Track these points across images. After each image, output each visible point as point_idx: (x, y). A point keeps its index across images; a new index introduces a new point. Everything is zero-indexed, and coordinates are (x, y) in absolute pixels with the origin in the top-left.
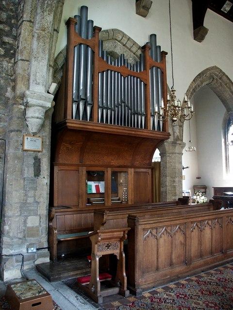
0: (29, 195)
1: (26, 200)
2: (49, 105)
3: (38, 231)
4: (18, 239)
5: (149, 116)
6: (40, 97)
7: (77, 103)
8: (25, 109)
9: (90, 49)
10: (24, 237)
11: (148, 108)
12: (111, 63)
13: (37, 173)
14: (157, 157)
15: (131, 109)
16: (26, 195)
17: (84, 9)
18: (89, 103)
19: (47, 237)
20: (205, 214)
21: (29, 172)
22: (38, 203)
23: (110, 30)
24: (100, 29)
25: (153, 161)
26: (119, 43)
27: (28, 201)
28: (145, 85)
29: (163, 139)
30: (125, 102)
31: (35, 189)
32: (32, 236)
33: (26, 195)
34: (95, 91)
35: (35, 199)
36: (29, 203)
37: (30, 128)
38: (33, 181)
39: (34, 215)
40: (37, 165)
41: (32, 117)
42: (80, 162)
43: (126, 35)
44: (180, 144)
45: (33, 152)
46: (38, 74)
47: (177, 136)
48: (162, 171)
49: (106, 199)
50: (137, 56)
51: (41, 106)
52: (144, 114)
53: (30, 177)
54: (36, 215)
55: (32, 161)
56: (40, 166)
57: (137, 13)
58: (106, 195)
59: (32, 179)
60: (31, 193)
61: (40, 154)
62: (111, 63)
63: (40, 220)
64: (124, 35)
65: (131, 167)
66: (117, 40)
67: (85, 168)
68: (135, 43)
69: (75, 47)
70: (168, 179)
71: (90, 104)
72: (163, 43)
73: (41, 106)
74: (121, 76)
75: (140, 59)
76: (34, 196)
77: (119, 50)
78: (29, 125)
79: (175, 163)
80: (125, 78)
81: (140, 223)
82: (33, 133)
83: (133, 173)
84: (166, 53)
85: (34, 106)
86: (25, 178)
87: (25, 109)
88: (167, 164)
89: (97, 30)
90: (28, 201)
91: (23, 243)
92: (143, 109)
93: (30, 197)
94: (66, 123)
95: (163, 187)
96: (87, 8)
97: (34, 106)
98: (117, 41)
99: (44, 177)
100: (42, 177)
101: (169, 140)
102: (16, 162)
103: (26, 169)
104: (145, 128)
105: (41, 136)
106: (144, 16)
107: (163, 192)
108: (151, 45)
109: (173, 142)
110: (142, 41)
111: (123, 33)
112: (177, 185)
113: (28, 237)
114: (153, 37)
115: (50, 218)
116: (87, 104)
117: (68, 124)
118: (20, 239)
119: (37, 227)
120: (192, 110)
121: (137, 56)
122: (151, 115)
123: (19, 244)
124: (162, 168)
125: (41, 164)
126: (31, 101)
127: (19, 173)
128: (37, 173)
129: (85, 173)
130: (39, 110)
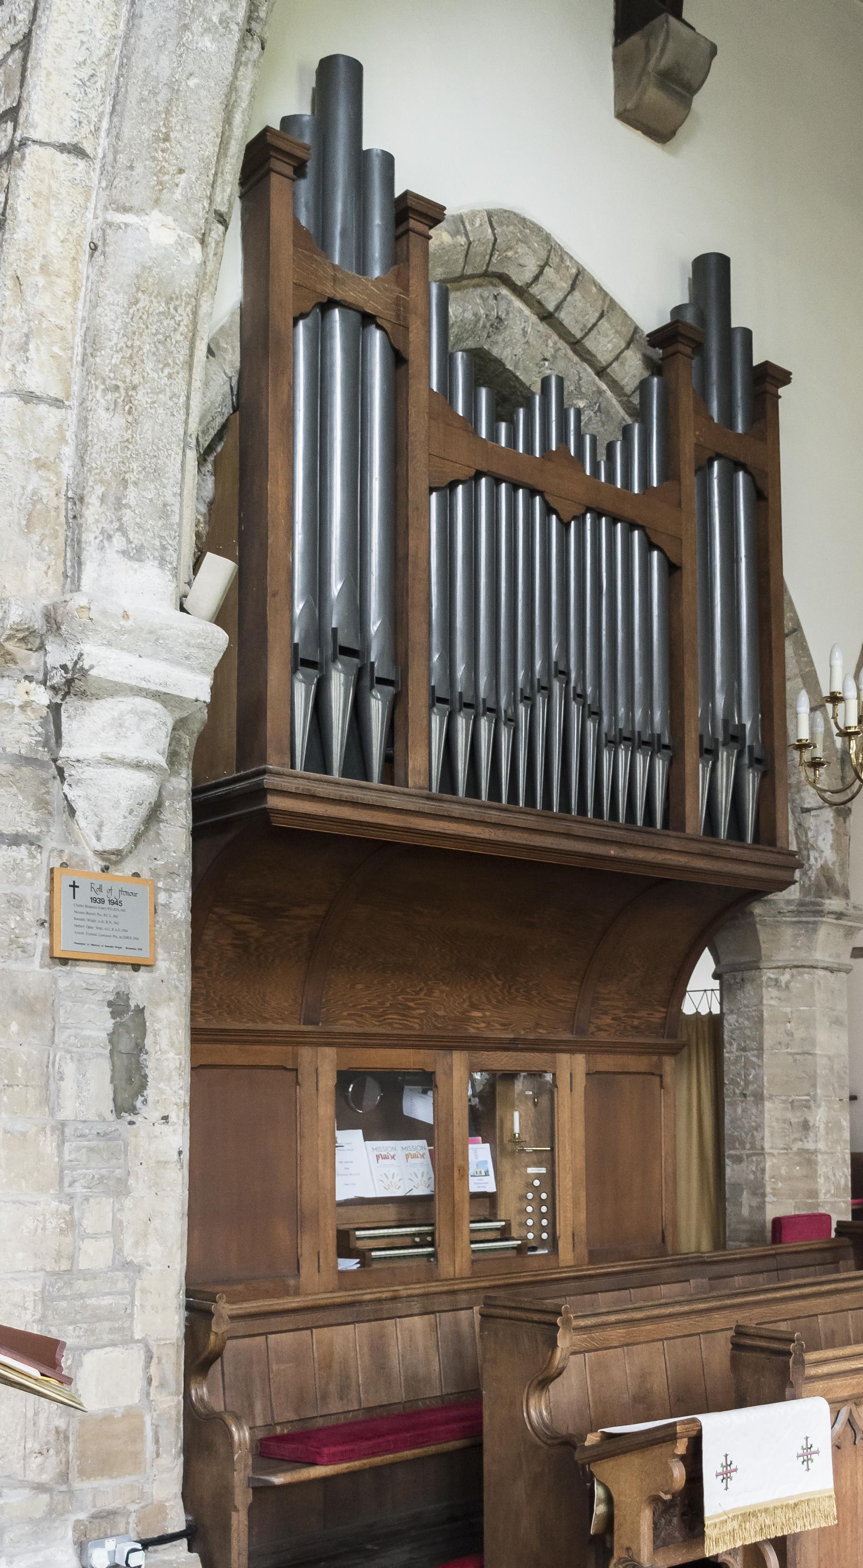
0: (89, 1223)
1: (72, 1258)
2: (198, 687)
3: (136, 1435)
4: (27, 1492)
5: (691, 753)
6: (153, 640)
7: (314, 673)
8: (55, 709)
9: (377, 338)
10: (64, 1477)
11: (688, 705)
12: (494, 434)
13: (130, 1087)
14: (701, 994)
15: (597, 714)
16: (71, 1225)
17: (339, 81)
18: (377, 674)
19: (182, 1459)
20: (520, 1277)
21: (87, 1088)
22: (132, 1269)
23: (474, 214)
24: (433, 214)
25: (688, 1009)
26: (518, 303)
27: (83, 1264)
28: (671, 569)
29: (751, 886)
30: (566, 673)
31: (120, 1188)
32: (105, 1465)
33: (71, 1225)
34: (692, 665)
35: (118, 1250)
36: (90, 1275)
37: (84, 822)
38: (111, 1145)
39: (115, 1345)
40: (125, 1044)
41: (110, 761)
42: (307, 1022)
43: (563, 255)
44: (840, 915)
45: (102, 971)
46: (132, 496)
47: (824, 869)
48: (730, 1070)
49: (443, 1235)
50: (614, 385)
51: (156, 696)
52: (666, 740)
53: (92, 1116)
54: (128, 1341)
55: (101, 1024)
56: (140, 1048)
57: (623, 115)
58: (439, 1207)
59: (102, 1128)
60: (97, 1214)
61: (142, 977)
62: (494, 434)
63: (147, 1365)
64: (552, 253)
65: (572, 1048)
66: (505, 280)
67: (330, 1053)
68: (609, 308)
69: (295, 324)
70: (772, 1111)
71: (381, 681)
72: (767, 316)
73: (156, 696)
74: (548, 510)
75: (641, 414)
76: (118, 1229)
77: (523, 346)
78: (80, 806)
79: (809, 1022)
80: (564, 526)
81: (811, 1371)
82: (101, 854)
83: (580, 1081)
84: (784, 377)
85: (115, 690)
86: (63, 1124)
87: (55, 709)
88: (767, 1027)
89: (413, 215)
90: (83, 1264)
91: (54, 1513)
92: (658, 715)
93: (95, 1236)
94: (261, 793)
95: (738, 1159)
96: (356, 69)
97: (115, 690)
98: (505, 291)
99: (165, 1118)
100: (158, 1115)
101: (40, 772)
102: (14, 1027)
103: (70, 1069)
104: (666, 824)
105: (145, 874)
106: (661, 132)
107: (738, 1188)
108: (702, 318)
109: (802, 904)
110: (651, 296)
111: (547, 238)
112: (821, 1146)
113: (83, 1473)
114: (712, 275)
115: (199, 1359)
116: (366, 682)
117: (274, 802)
118: (40, 1488)
119: (130, 1413)
120: (851, 718)
121: (614, 385)
122: (300, 662)
123: (31, 1520)
124: (730, 1052)
125: (148, 1042)
126: (104, 661)
127: (32, 1095)
128: (130, 1087)
129: (328, 1081)
130: (142, 716)
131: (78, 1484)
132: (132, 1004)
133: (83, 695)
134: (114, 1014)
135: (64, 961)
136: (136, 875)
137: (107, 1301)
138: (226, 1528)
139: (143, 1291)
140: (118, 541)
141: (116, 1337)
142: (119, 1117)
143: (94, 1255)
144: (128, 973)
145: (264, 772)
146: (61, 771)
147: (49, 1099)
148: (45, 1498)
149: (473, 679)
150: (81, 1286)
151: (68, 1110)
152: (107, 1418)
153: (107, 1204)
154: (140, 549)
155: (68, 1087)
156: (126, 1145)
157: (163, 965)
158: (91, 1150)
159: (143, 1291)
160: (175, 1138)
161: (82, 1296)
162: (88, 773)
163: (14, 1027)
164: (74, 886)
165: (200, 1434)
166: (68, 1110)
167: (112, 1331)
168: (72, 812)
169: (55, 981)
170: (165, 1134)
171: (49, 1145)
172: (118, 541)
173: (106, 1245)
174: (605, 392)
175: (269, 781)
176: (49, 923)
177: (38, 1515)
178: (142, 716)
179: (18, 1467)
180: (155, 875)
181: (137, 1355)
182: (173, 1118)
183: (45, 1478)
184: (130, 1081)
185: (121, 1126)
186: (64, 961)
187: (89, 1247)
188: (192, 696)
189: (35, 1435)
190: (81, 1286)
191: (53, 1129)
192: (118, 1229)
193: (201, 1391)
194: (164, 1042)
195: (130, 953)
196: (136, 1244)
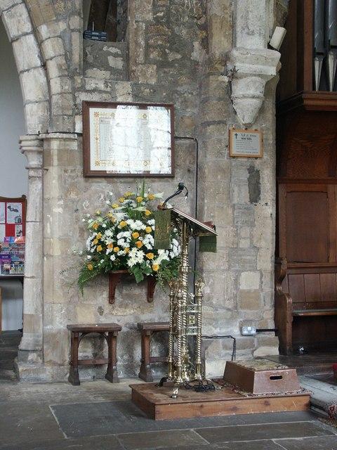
0: (243, 234)
2: (272, 71)
3: (258, 298)
10: (236, 307)
13: (255, 196)
21: (241, 195)
31: (252, 225)
32: (248, 306)
33: (237, 235)
35: (251, 243)
37: (239, 116)
39: (250, 271)
45: (246, 160)
51: (259, 75)
55: (245, 175)
60: (245, 232)
61: (258, 161)
63: (261, 278)
76: (251, 237)
78: (238, 111)
82: (245, 125)
85: (246, 75)
86: (234, 205)
93: (244, 238)
97: (246, 75)
99: (266, 204)
103: (236, 189)
105: (259, 129)
115: (279, 278)
117: (306, 102)
126: (242, 67)
127: (225, 197)
128: (255, 196)
130: (255, 82)
131: (240, 310)
132: (255, 169)
133: (237, 78)
134: (249, 173)
135: (234, 157)
136: (256, 130)
137: (248, 257)
138: (285, 330)
139: (260, 256)
140: (246, 30)
141: (251, 268)
142: (251, 203)
143: (244, 244)
144: (254, 160)
145: (302, 93)
146: (232, 101)
147: (230, 198)
148: (230, 313)
149: (131, 180)
150: (240, 252)
151: (235, 201)
152: (249, 292)
153: (248, 229)
154: (253, 32)
155: (236, 194)
156: (254, 211)
157: (266, 157)
158: (243, 213)
159: (260, 256)
160: (270, 210)
161: (241, 256)
162: (239, 101)
163: (219, 177)
164: (236, 135)
165: (279, 301)
166: (235, 201)
167: (250, 266)
168: (236, 113)
169: (231, 163)
170: (267, 209)
171: (230, 212)
172: (246, 30)
173: (248, 241)
174: (60, 239)
175: (303, 96)
176: (229, 146)
177: (228, 317)
178: (255, 82)
179: (222, 303)
180: (262, 129)
181: (257, 275)
182: (269, 204)
183: (230, 307)
184: (255, 192)
185: (252, 206)
186: (234, 157)
187: (243, 241)
188: (270, 74)
189: (227, 294)
190: (240, 252)
191: (231, 207)
192: (251, 237)
193: (279, 288)
194: (266, 181)
195: (255, 154)
196: (257, 242)
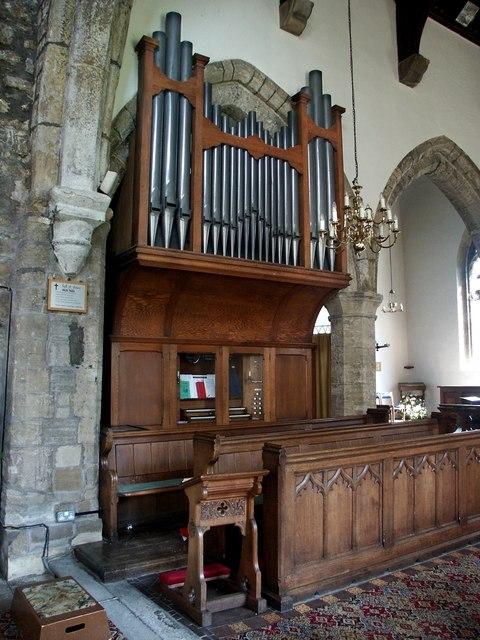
0: (61, 402)
1: (54, 414)
2: (101, 216)
3: (78, 476)
4: (37, 494)
5: (307, 239)
6: (83, 201)
7: (158, 213)
8: (52, 225)
9: (185, 102)
10: (50, 489)
11: (306, 223)
12: (229, 131)
13: (77, 356)
14: (322, 324)
15: (270, 226)
16: (53, 403)
17: (173, 19)
18: (183, 212)
19: (96, 489)
20: (422, 441)
21: (60, 356)
22: (79, 419)
23: (226, 62)
24: (206, 60)
25: (315, 332)
26: (245, 89)
27: (58, 416)
28: (299, 176)
29: (336, 286)
30: (257, 212)
31: (73, 391)
32: (67, 486)
33: (53, 403)
34: (197, 188)
35: (71, 411)
36: (60, 420)
37: (61, 264)
38: (68, 374)
39: (70, 445)
40: (76, 340)
41: (67, 242)
42: (165, 335)
43: (260, 73)
44: (371, 298)
45: (67, 315)
46: (78, 153)
47: (365, 280)
48: (333, 353)
49: (218, 411)
50: (281, 115)
51: (85, 220)
52: (298, 234)
53: (61, 365)
54: (75, 443)
55: (66, 333)
56: (81, 342)
57: (282, 27)
58: (218, 403)
59: (66, 369)
60: (64, 399)
61: (82, 317)
62: (229, 131)
63: (82, 453)
64: (255, 72)
65: (270, 345)
66: (241, 83)
67: (175, 346)
68: (277, 89)
69: (154, 97)
70: (347, 369)
71: (185, 215)
72: (335, 89)
73: (85, 220)
74: (250, 156)
75: (289, 122)
76: (71, 406)
77: (245, 103)
78: (59, 258)
79: (360, 336)
80: (257, 162)
81: (288, 461)
82: (68, 274)
83: (274, 358)
84: (343, 110)
85: (70, 218)
86: (51, 367)
87: (52, 225)
88: (345, 338)
89: (199, 61)
90: (58, 416)
91: (46, 502)
92: (294, 226)
93: (62, 407)
94: (136, 254)
95: (335, 386)
96: (179, 16)
97: (70, 218)
98: (240, 86)
99: (91, 366)
100: (87, 365)
101: (349, 289)
102: (33, 334)
103: (54, 348)
104: (298, 264)
105: (85, 280)
106: (298, 33)
107: (335, 396)
108: (312, 93)
109: (356, 293)
110: (292, 85)
111: (254, 68)
112: (365, 381)
113: (57, 489)
114: (315, 76)
115: (104, 451)
116: (179, 215)
117: (140, 257)
118: (42, 493)
119: (75, 468)
120: (396, 227)
121: (281, 115)
122: (312, 238)
123: (38, 504)
124: (333, 347)
125: (84, 339)
126: (64, 208)
127: (39, 357)
128: (77, 356)
129: (174, 356)
130: (80, 227)
